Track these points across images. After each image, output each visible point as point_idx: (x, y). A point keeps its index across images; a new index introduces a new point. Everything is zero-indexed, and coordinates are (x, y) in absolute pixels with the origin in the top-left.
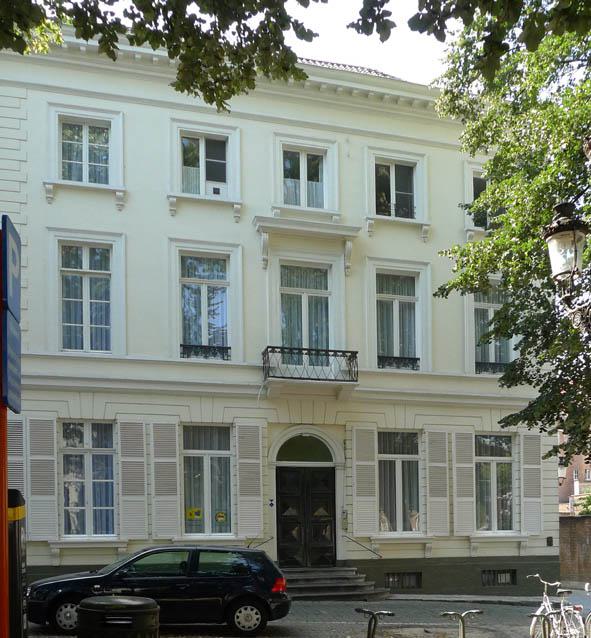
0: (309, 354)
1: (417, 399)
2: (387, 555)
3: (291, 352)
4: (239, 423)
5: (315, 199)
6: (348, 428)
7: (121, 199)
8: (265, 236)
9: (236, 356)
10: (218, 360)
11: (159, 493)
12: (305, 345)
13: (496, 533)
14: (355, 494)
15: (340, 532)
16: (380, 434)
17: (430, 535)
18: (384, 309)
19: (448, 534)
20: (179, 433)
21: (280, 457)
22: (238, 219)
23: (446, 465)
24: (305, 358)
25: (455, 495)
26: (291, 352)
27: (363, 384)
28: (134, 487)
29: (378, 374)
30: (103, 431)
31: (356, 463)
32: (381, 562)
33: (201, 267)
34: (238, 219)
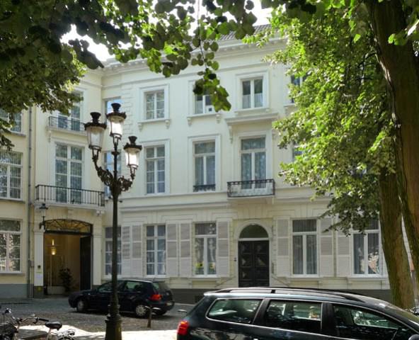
3: (246, 183)
4: (219, 220)
5: (258, 103)
6: (274, 219)
7: (168, 123)
8: (230, 127)
9: (218, 189)
10: (210, 191)
13: (305, 275)
15: (271, 274)
19: (332, 276)
20: (290, 223)
21: (242, 235)
22: (219, 122)
23: (176, 241)
25: (337, 252)
26: (246, 183)
27: (280, 195)
29: (147, 198)
30: (162, 228)
33: (204, 148)
34: (219, 122)
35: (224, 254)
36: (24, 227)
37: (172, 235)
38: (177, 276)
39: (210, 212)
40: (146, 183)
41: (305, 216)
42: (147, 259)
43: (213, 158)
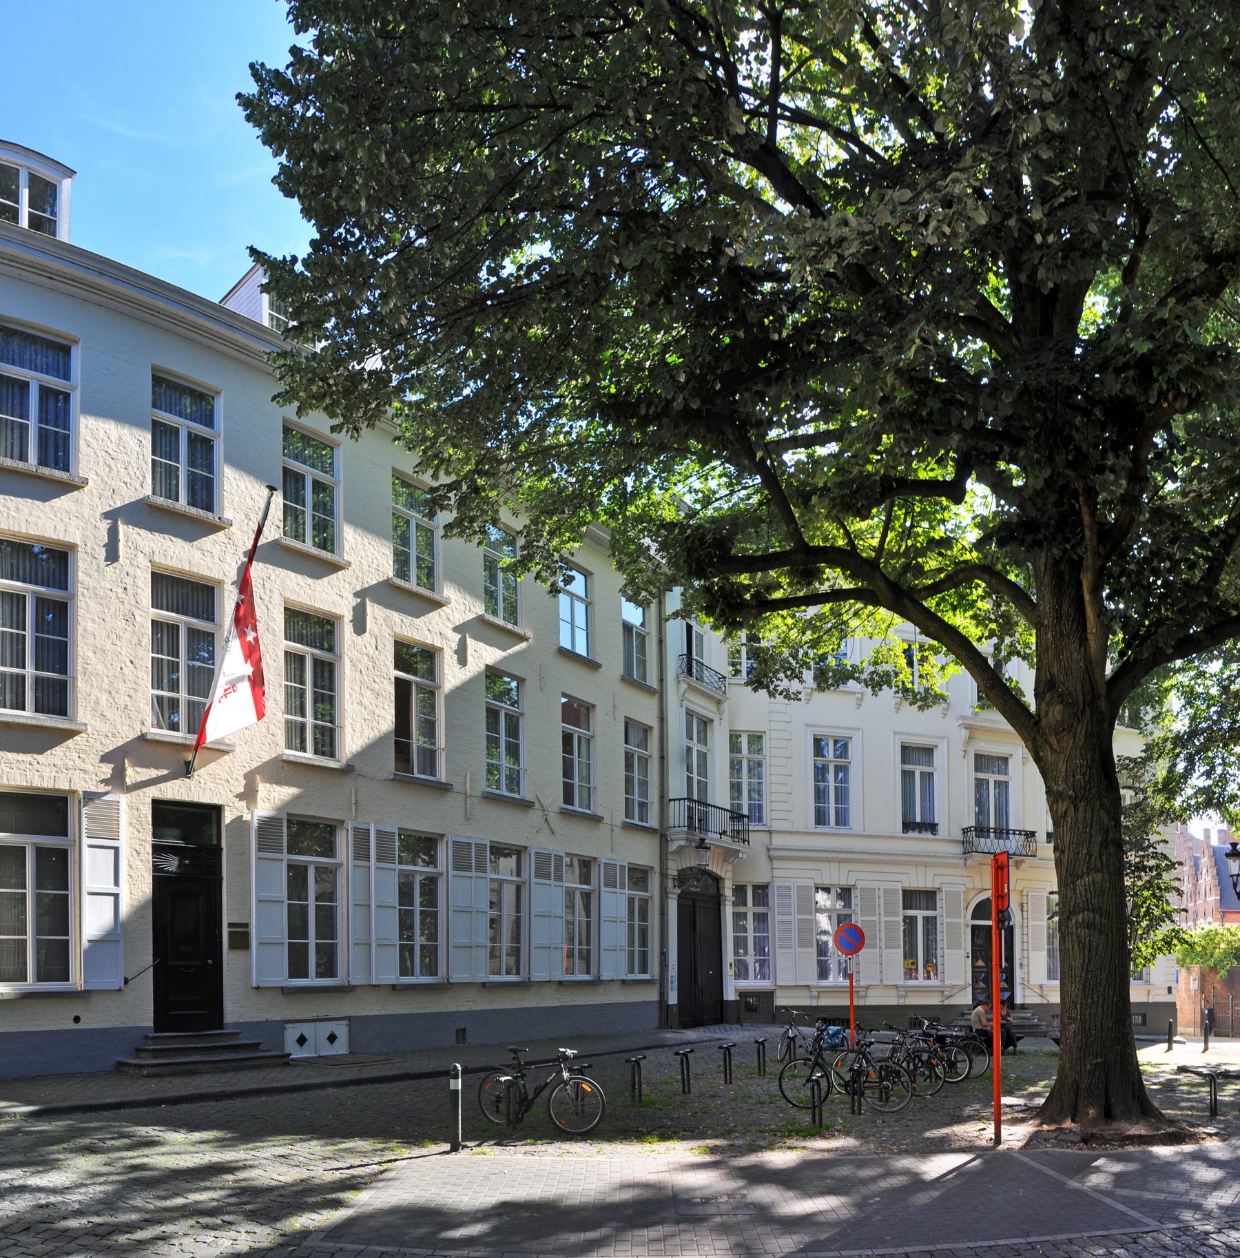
2: (824, 1002)
3: (981, 830)
4: (860, 884)
9: (942, 830)
12: (992, 825)
16: (904, 891)
18: (907, 776)
19: (112, 898)
23: (876, 918)
24: (992, 835)
29: (816, 834)
35: (954, 945)
36: (654, 881)
37: (869, 909)
38: (878, 983)
39: (845, 867)
43: (931, 775)
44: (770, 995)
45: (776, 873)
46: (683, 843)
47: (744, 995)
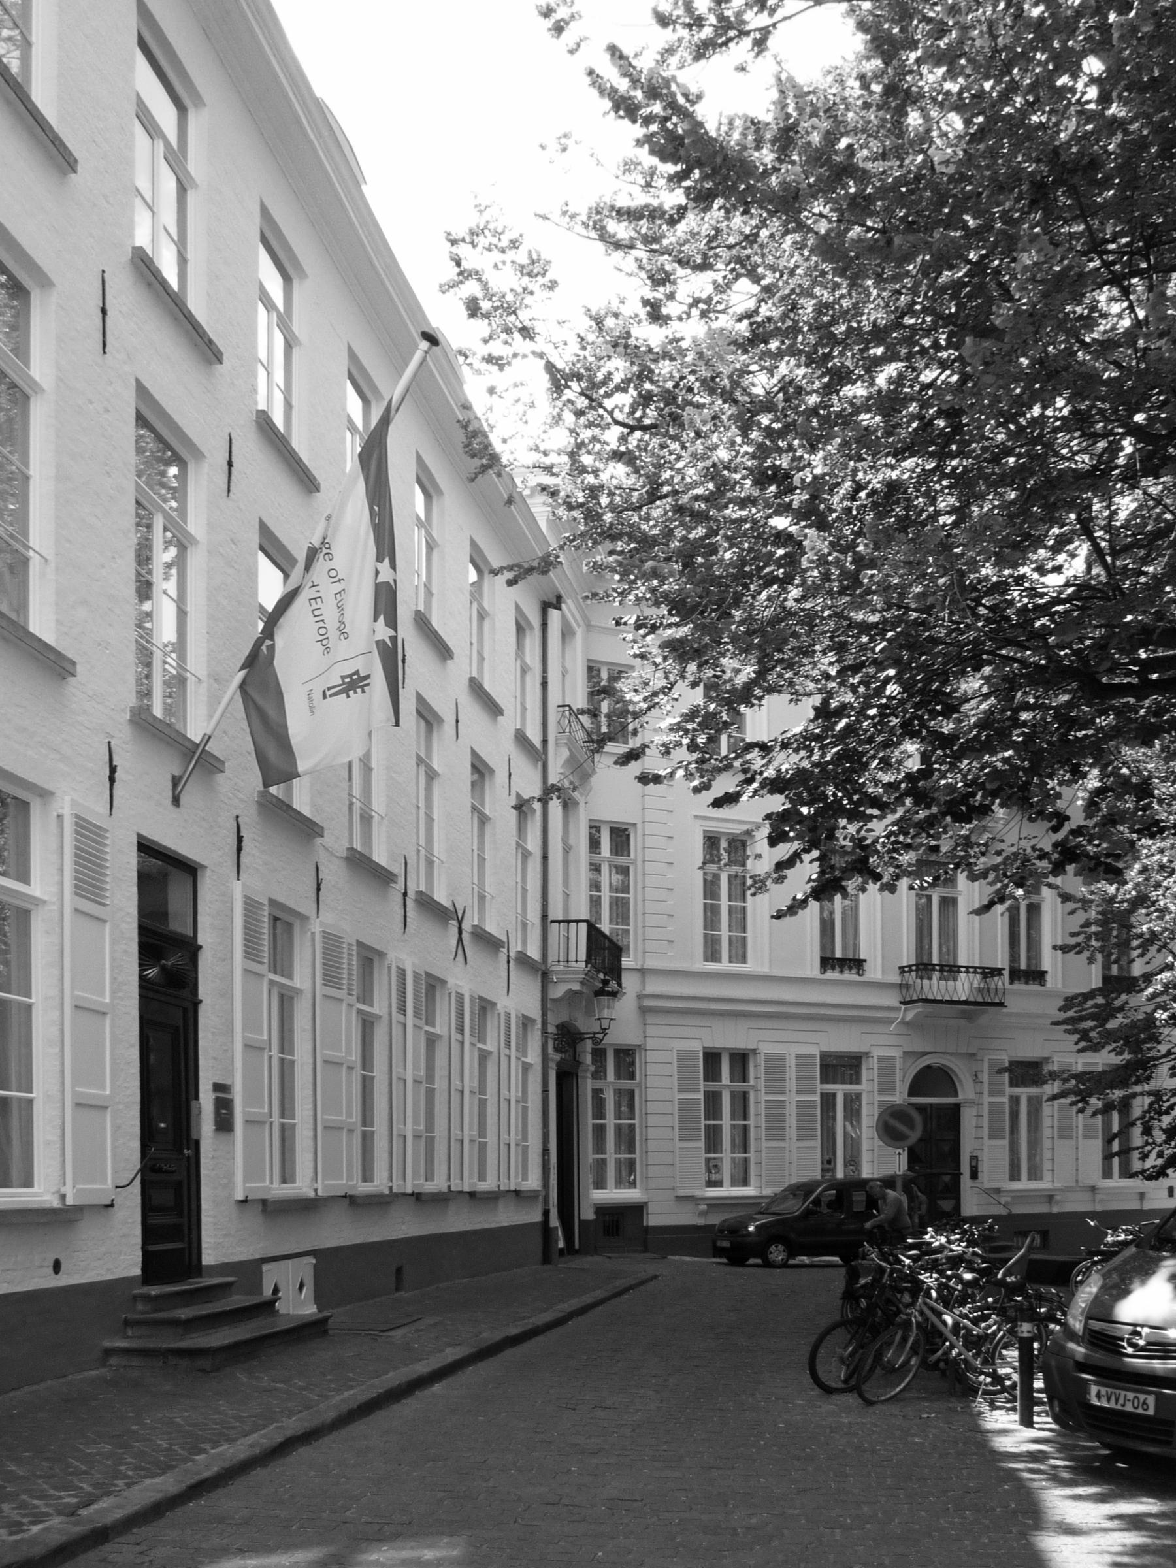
0: (941, 971)
1: (822, 1011)
2: (1018, 1210)
3: (923, 967)
4: (877, 1052)
9: (874, 972)
11: (800, 1138)
12: (935, 960)
14: (986, 1137)
17: (1058, 1185)
28: (776, 1131)
30: (741, 1059)
31: (764, 1097)
32: (1011, 1217)
40: (749, 934)
41: (651, 1069)
42: (1108, 1157)
44: (637, 1210)
45: (651, 1031)
46: (576, 987)
47: (602, 1210)
